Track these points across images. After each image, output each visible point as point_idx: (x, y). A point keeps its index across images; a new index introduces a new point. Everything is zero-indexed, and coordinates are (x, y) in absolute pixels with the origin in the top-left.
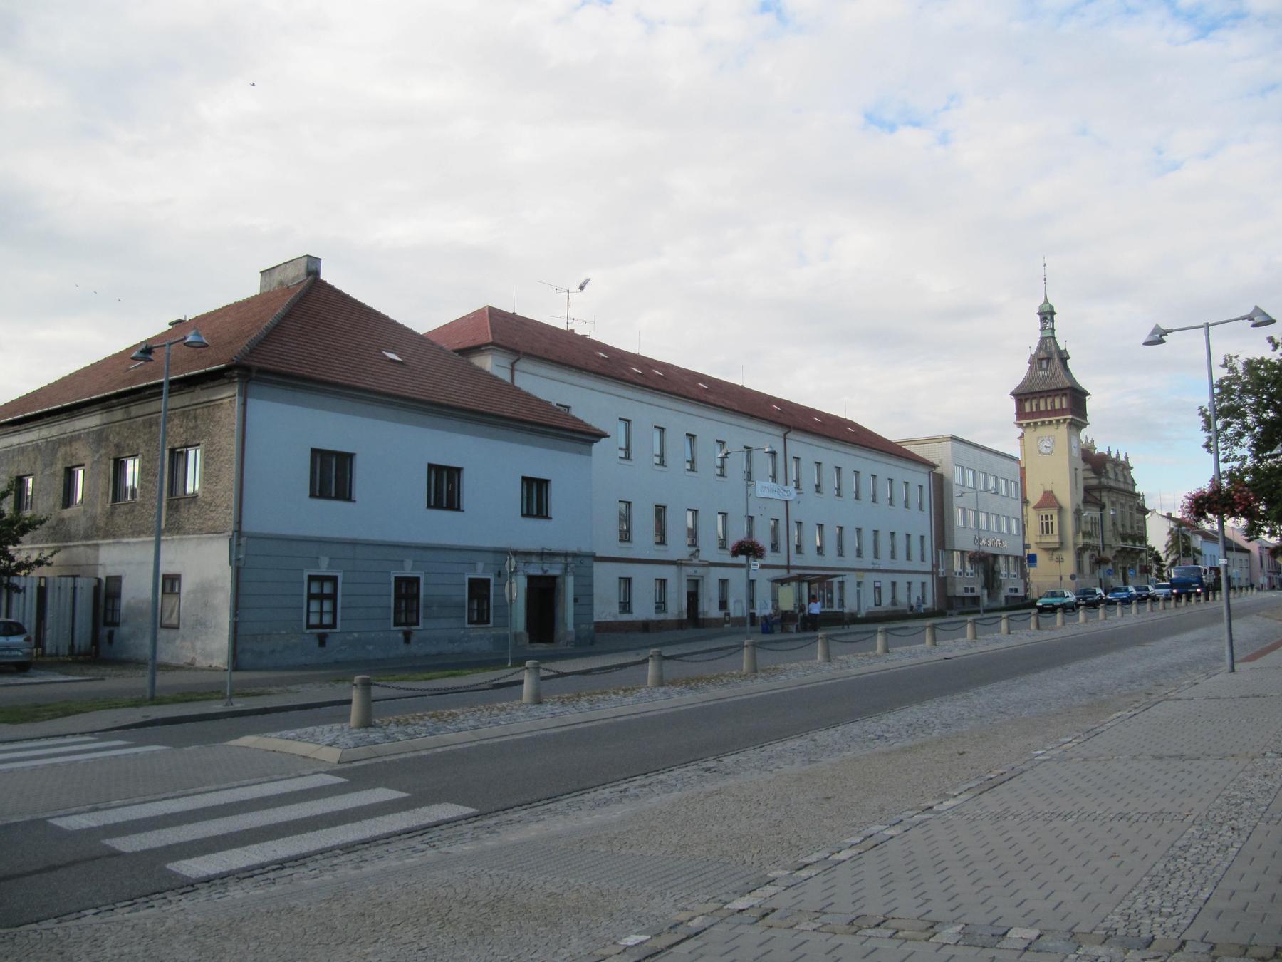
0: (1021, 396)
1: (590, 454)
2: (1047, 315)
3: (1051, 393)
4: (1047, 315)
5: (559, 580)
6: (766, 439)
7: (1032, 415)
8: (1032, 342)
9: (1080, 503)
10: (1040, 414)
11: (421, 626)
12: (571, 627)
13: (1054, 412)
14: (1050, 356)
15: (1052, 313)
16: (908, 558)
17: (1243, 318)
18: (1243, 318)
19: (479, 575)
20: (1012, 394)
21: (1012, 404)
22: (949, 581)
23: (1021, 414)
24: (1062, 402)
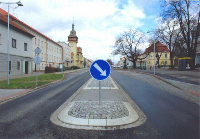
0: (69, 37)
1: (32, 39)
2: (73, 25)
3: (73, 38)
4: (73, 25)
5: (29, 62)
6: (44, 41)
7: (71, 40)
8: (71, 30)
9: (77, 50)
10: (72, 40)
11: (11, 71)
12: (30, 71)
13: (74, 40)
14: (73, 32)
15: (74, 25)
16: (54, 61)
17: (16, 3)
18: (16, 3)
19: (19, 61)
20: (68, 37)
21: (68, 38)
22: (68, 58)
23: (69, 40)
24: (75, 39)
